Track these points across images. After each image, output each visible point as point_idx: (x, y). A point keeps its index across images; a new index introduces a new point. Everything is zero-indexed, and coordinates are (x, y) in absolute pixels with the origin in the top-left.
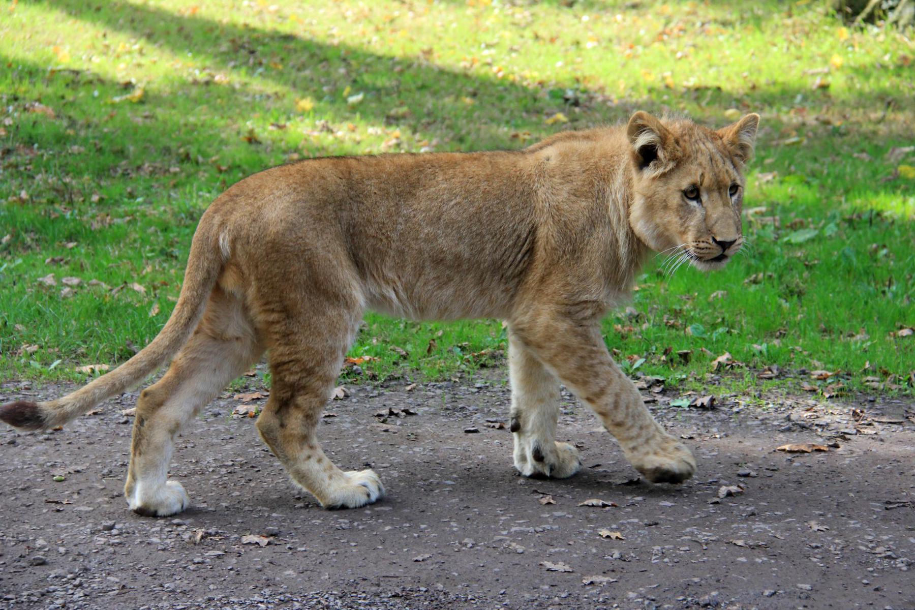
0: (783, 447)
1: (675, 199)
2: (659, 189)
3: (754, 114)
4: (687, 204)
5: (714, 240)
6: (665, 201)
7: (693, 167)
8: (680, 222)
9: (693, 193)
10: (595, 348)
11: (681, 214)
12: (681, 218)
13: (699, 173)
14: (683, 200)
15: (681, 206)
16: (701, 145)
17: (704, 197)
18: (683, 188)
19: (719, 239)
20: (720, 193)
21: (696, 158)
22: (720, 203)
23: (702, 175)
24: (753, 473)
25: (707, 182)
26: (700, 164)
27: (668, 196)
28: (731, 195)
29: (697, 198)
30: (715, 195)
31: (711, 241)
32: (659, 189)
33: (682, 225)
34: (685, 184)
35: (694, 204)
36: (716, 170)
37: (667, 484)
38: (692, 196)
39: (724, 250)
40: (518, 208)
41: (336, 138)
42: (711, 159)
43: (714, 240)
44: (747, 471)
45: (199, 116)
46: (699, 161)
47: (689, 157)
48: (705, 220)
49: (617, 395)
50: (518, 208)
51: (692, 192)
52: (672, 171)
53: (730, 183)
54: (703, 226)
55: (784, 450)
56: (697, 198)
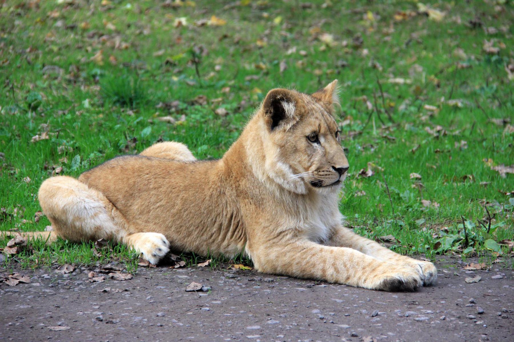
1: (303, 144)
4: (311, 145)
5: (334, 168)
7: (312, 120)
8: (308, 159)
10: (431, 178)
12: (309, 156)
14: (309, 143)
15: (308, 146)
17: (322, 140)
18: (307, 135)
19: (337, 167)
23: (319, 125)
25: (323, 130)
26: (317, 118)
29: (317, 141)
30: (330, 137)
33: (309, 161)
34: (308, 131)
35: (315, 145)
37: (247, 267)
38: (313, 140)
40: (211, 208)
49: (334, 265)
50: (211, 208)
51: (313, 137)
54: (324, 159)
56: (317, 141)
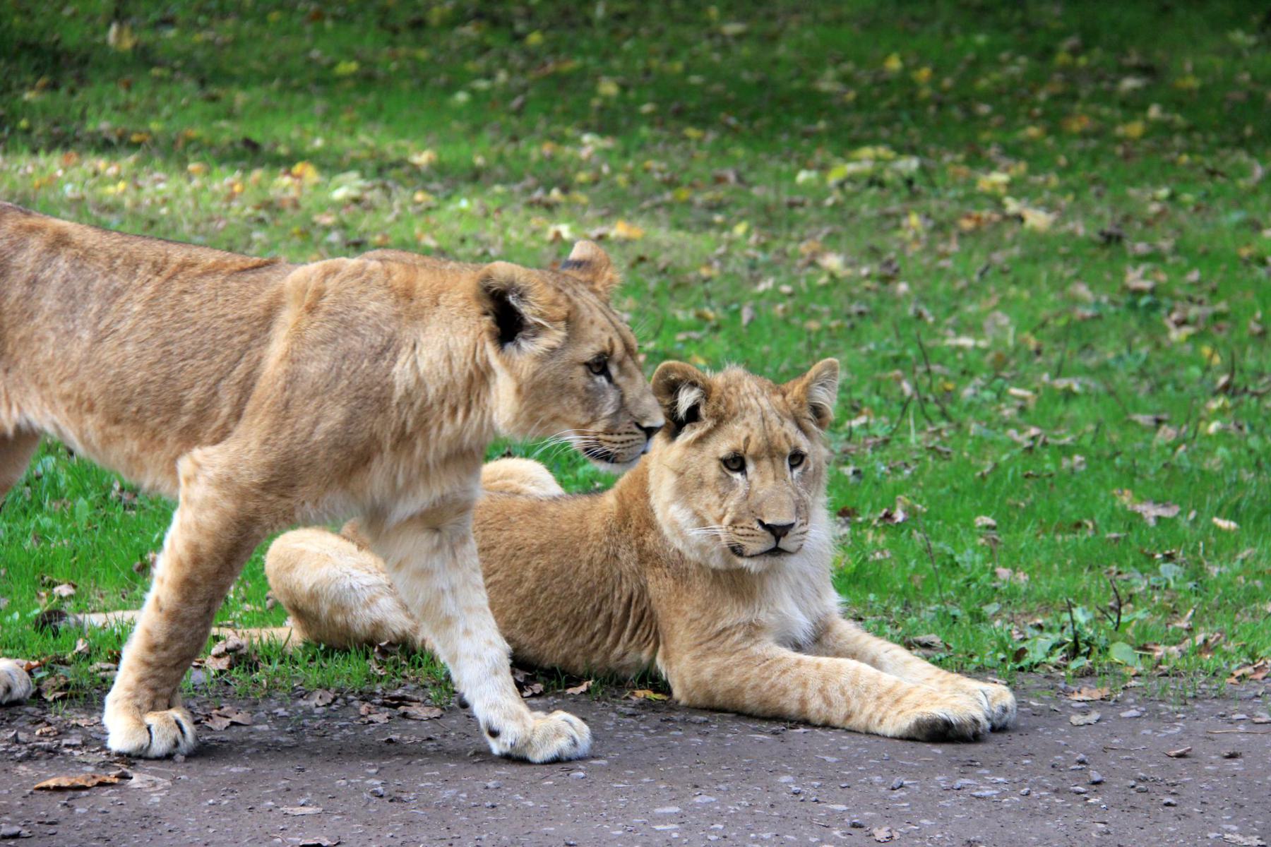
0: (44, 784)
1: (712, 471)
2: (692, 460)
3: (829, 359)
5: (761, 523)
6: (700, 476)
9: (735, 463)
11: (721, 489)
12: (720, 496)
13: (743, 437)
16: (753, 401)
17: (751, 468)
19: (767, 521)
20: (773, 462)
21: (743, 417)
22: (771, 474)
24: (25, 832)
26: (748, 425)
27: (703, 468)
28: (792, 467)
29: (742, 468)
30: (766, 464)
31: (756, 525)
32: (692, 460)
33: (721, 506)
35: (737, 476)
36: (769, 434)
38: (735, 467)
39: (778, 540)
41: (973, 437)
42: (763, 419)
43: (761, 523)
44: (16, 829)
45: (536, 379)
46: (746, 421)
47: (735, 415)
48: (747, 497)
52: (709, 433)
53: (788, 451)
55: (47, 788)
56: (742, 468)
